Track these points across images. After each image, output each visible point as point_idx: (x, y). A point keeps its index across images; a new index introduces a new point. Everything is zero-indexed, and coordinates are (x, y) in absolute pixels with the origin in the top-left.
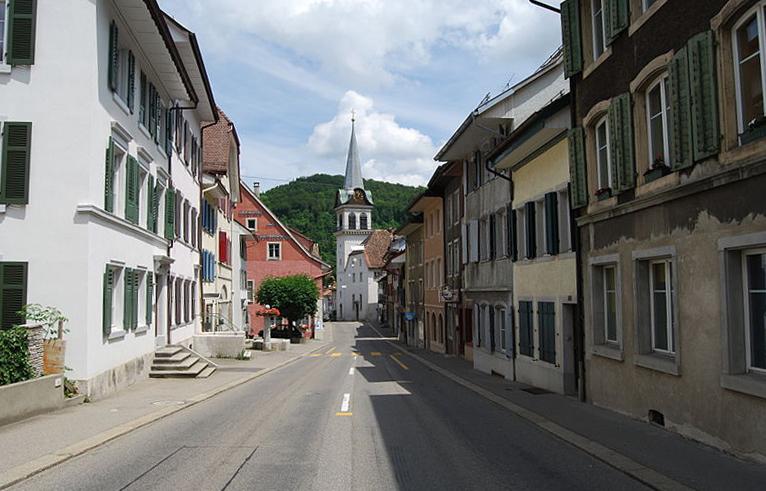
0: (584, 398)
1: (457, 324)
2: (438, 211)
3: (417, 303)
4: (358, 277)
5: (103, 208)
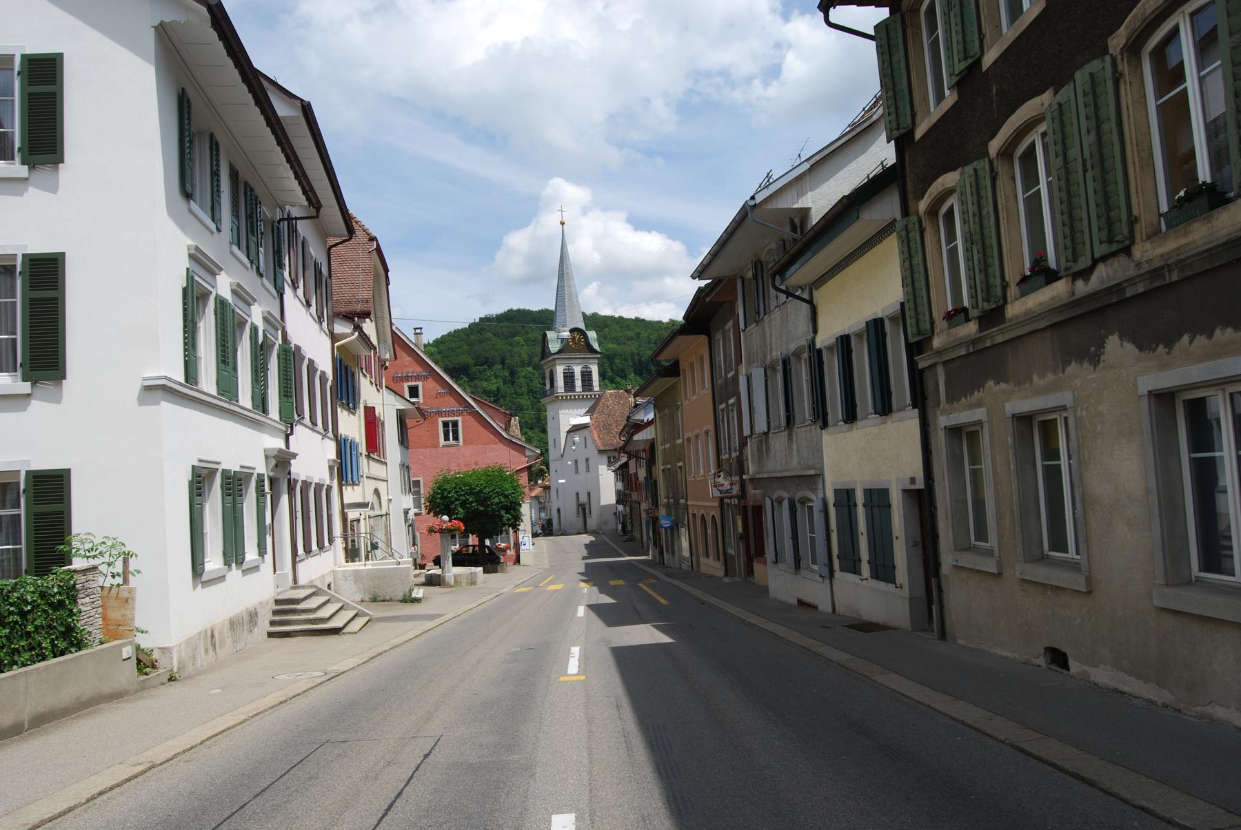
0: (943, 635)
1: (740, 530)
2: (702, 357)
3: (677, 502)
4: (582, 465)
5: (182, 380)
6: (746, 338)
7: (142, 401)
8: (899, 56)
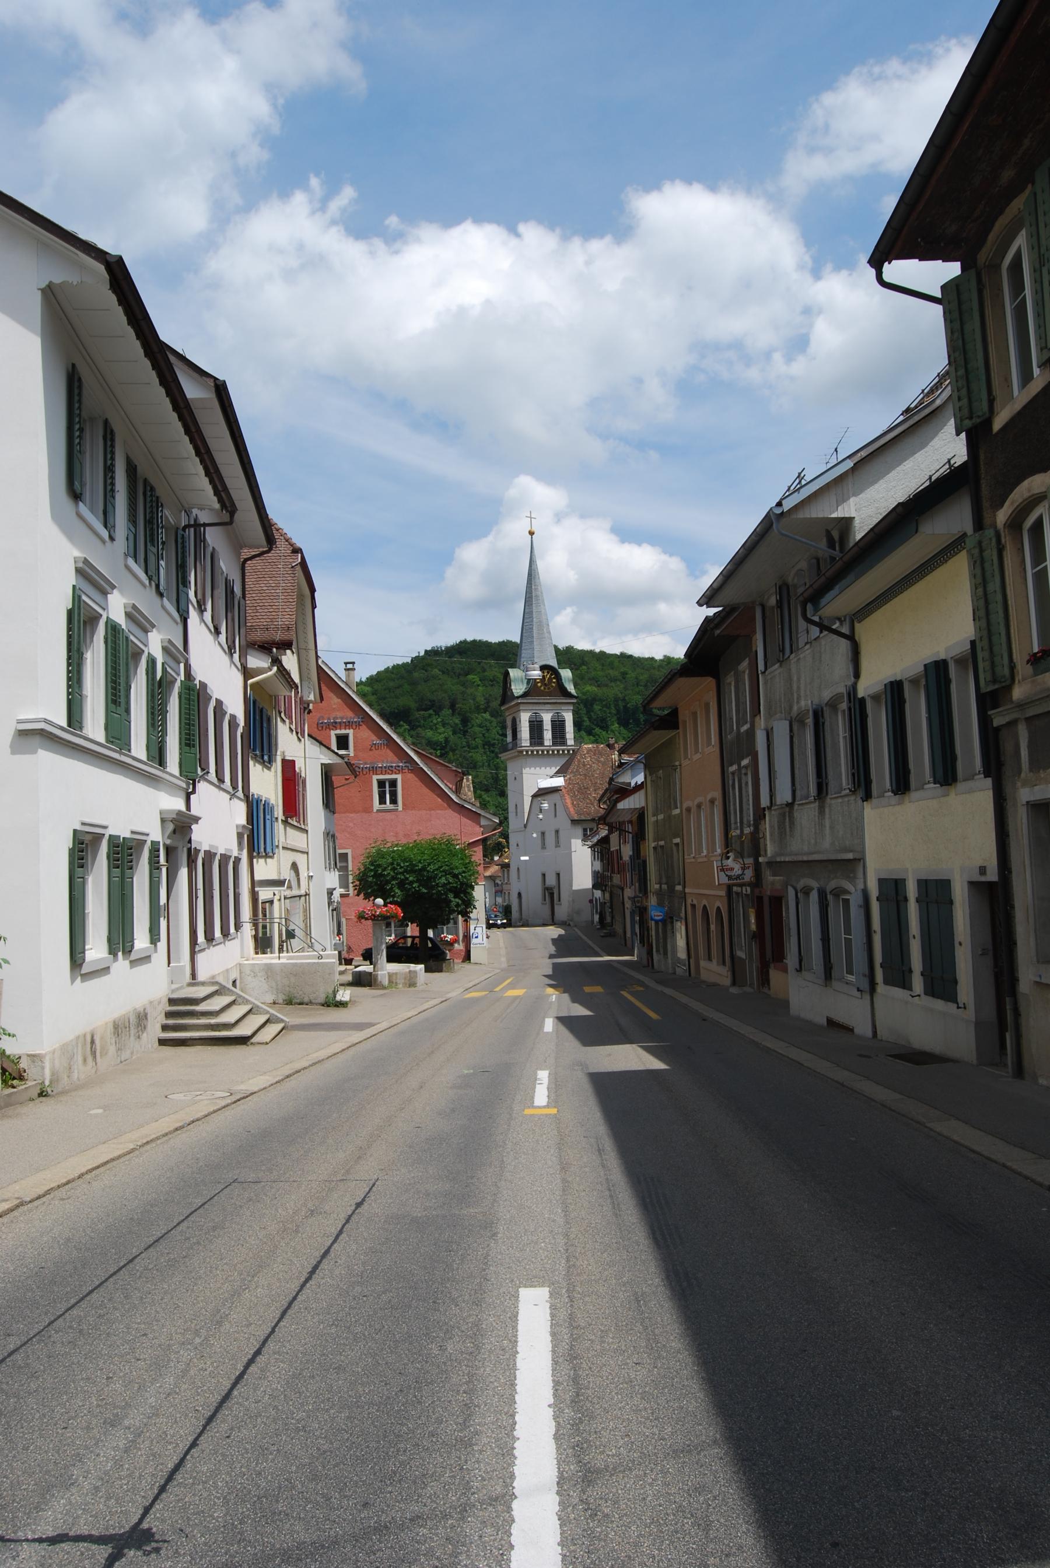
0: (1019, 1071)
1: (753, 927)
2: (707, 705)
4: (550, 839)
5: (64, 724)
6: (766, 683)
7: (15, 749)
8: (973, 324)
